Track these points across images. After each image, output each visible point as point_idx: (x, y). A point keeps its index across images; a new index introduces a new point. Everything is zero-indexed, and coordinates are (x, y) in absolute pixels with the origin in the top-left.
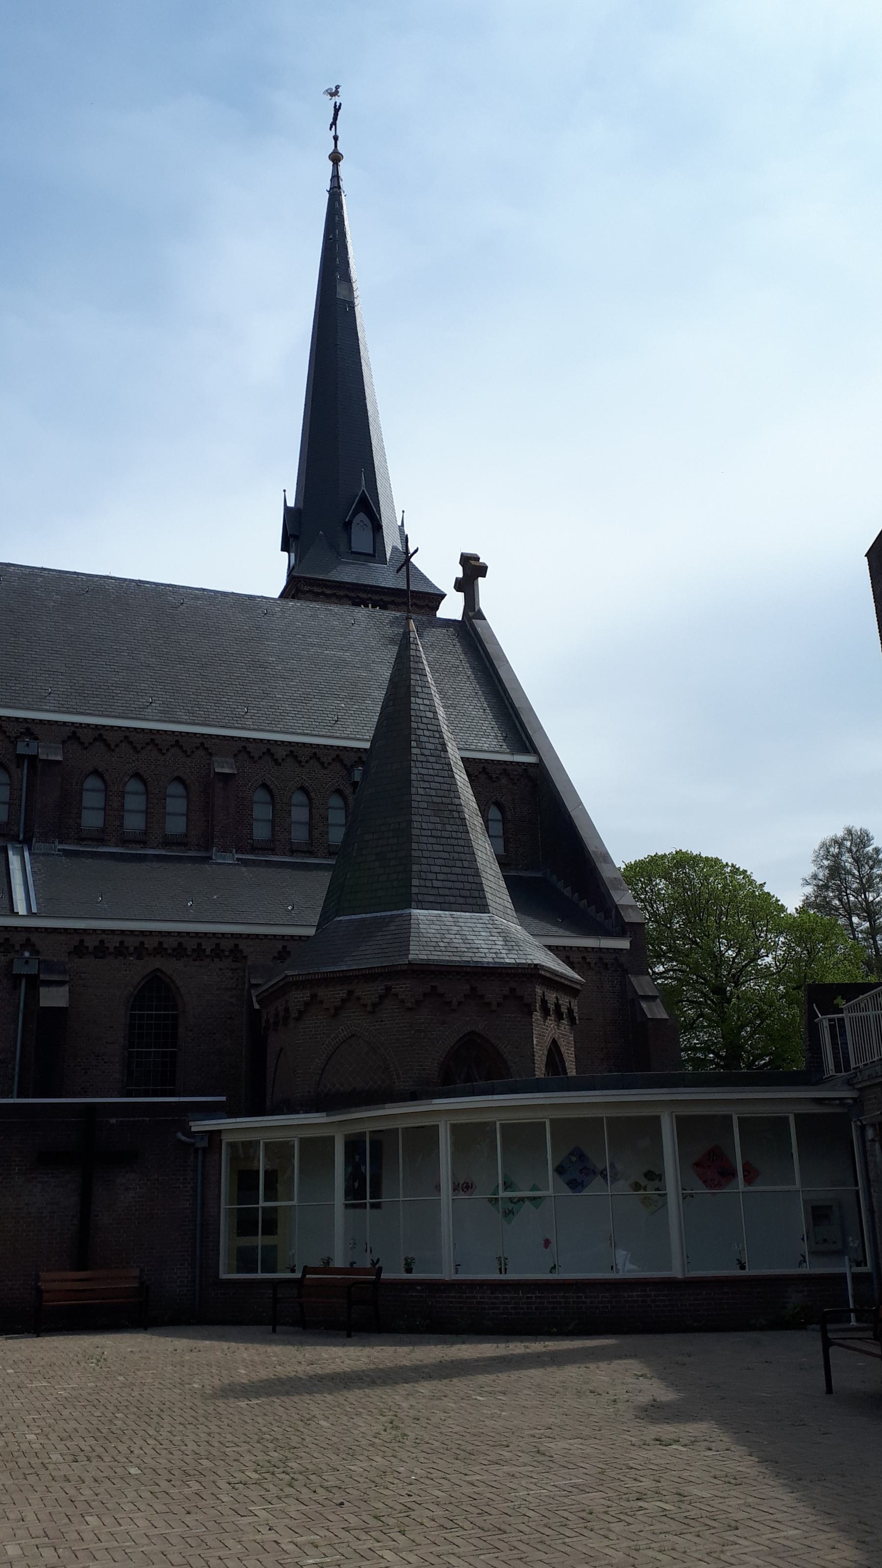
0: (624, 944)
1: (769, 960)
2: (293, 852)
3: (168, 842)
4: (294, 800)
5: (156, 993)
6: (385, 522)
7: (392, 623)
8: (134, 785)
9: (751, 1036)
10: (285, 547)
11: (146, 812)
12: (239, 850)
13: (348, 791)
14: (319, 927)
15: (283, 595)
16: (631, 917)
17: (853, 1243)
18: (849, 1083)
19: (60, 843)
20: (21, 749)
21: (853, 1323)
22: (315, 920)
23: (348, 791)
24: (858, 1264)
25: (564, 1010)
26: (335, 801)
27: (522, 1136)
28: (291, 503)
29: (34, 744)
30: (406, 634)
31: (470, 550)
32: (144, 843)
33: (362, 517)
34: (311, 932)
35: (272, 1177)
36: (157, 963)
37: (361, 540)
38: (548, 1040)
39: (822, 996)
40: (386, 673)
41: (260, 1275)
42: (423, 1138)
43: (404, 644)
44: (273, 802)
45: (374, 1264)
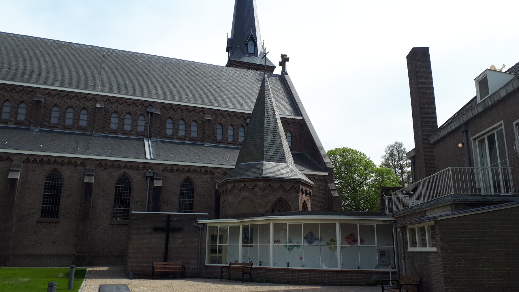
0: (326, 174)
1: (370, 180)
2: (228, 144)
3: (191, 140)
4: (229, 128)
5: (188, 184)
6: (258, 44)
7: (259, 75)
8: (181, 122)
9: (363, 203)
10: (227, 51)
11: (222, 134)
12: (213, 143)
13: (245, 126)
14: (236, 166)
15: (227, 66)
16: (329, 166)
17: (392, 262)
18: (393, 216)
19: (41, 128)
20: (148, 110)
21: (391, 285)
22: (235, 164)
23: (245, 126)
24: (393, 269)
25: (308, 192)
26: (241, 129)
27: (295, 228)
28: (230, 37)
29: (152, 109)
30: (264, 79)
31: (284, 53)
32: (184, 140)
33: (251, 42)
34: (234, 167)
35: (221, 237)
36: (126, 170)
37: (251, 49)
38: (303, 201)
39: (386, 190)
40: (257, 90)
41: (217, 265)
42: (266, 227)
43: (264, 81)
44: (223, 129)
45: (250, 263)
